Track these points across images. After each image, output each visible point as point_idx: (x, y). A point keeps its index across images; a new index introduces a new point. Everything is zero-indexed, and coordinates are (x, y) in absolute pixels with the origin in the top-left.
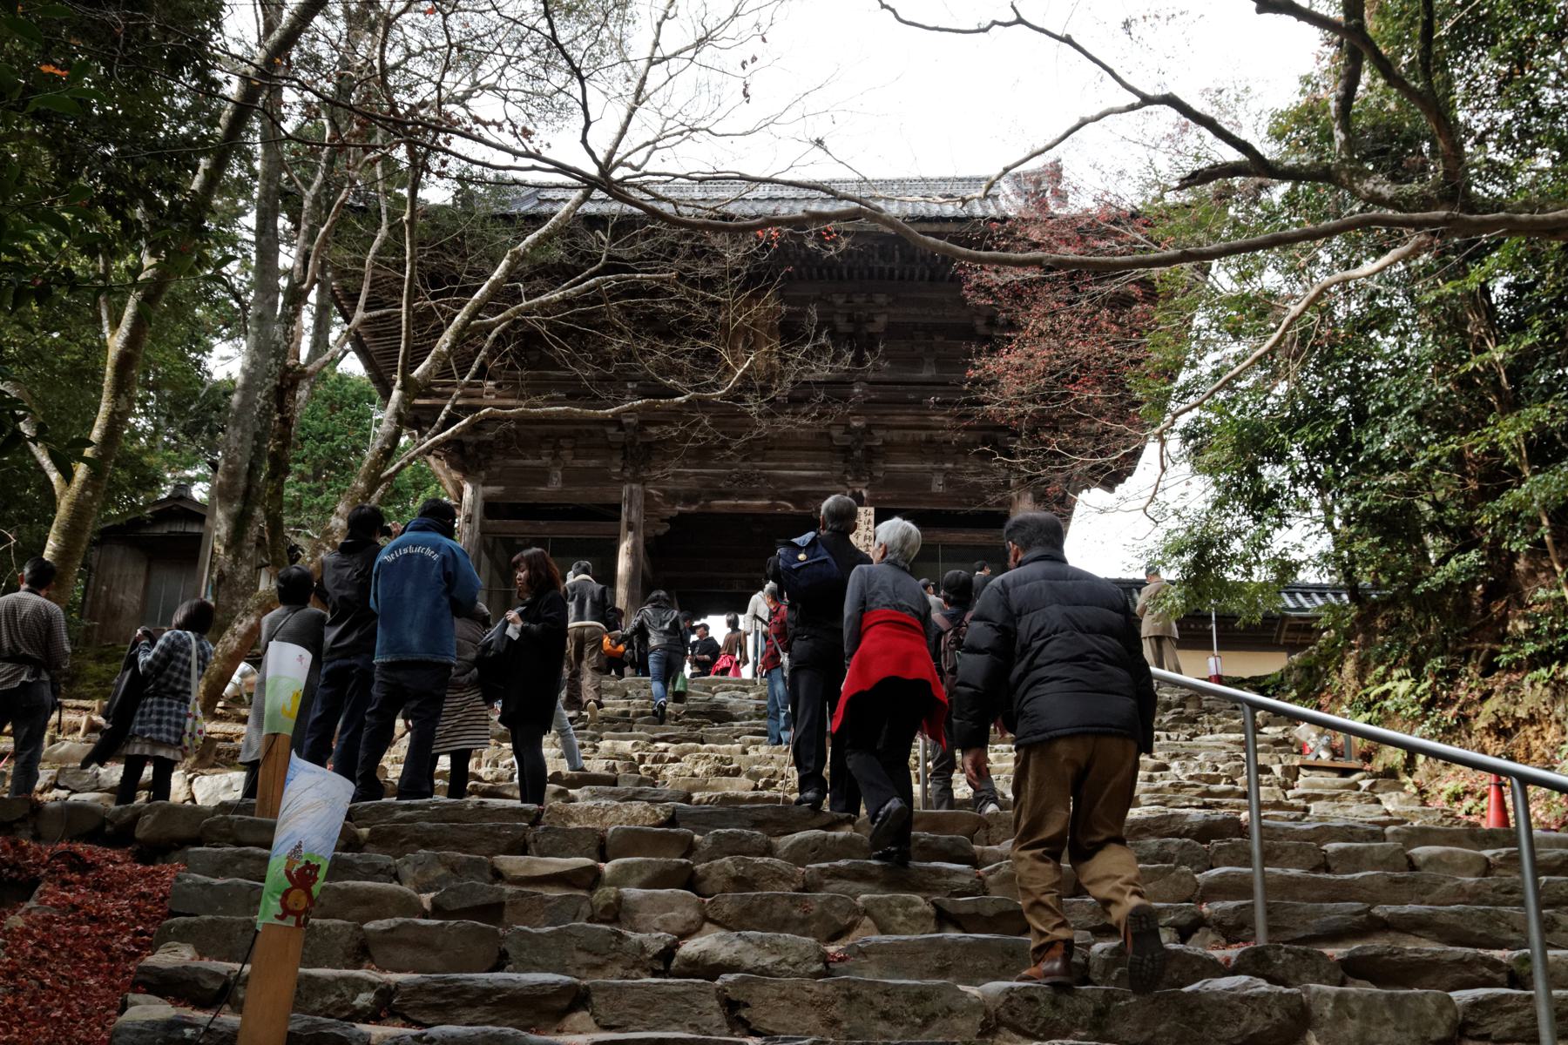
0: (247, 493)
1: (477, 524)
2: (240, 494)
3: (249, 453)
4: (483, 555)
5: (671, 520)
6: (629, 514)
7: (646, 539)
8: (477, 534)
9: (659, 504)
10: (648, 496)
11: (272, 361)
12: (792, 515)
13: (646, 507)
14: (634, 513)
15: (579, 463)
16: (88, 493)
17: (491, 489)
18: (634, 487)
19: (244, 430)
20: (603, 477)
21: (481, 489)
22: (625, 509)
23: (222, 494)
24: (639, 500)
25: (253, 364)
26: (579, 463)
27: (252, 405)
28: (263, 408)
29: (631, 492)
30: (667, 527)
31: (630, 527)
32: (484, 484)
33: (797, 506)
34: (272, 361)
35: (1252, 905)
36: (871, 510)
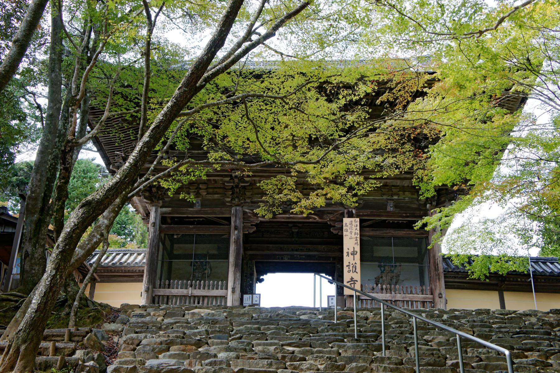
0: (42, 210)
1: (158, 227)
2: (38, 210)
3: (43, 188)
4: (160, 243)
5: (257, 225)
6: (235, 221)
7: (245, 235)
8: (158, 232)
9: (250, 217)
10: (245, 213)
11: (57, 139)
12: (317, 223)
13: (243, 218)
14: (238, 221)
15: (209, 197)
16: (145, 150)
17: (164, 210)
18: (238, 208)
19: (41, 175)
20: (223, 204)
21: (160, 210)
22: (233, 219)
23: (27, 211)
24: (240, 215)
25: (48, 140)
26: (209, 197)
27: (46, 162)
28: (51, 164)
29: (236, 210)
30: (255, 229)
31: (236, 228)
32: (161, 207)
33: (320, 218)
34: (57, 139)
35: (13, 234)
36: (358, 219)
